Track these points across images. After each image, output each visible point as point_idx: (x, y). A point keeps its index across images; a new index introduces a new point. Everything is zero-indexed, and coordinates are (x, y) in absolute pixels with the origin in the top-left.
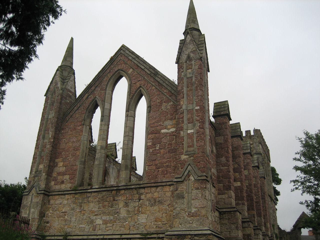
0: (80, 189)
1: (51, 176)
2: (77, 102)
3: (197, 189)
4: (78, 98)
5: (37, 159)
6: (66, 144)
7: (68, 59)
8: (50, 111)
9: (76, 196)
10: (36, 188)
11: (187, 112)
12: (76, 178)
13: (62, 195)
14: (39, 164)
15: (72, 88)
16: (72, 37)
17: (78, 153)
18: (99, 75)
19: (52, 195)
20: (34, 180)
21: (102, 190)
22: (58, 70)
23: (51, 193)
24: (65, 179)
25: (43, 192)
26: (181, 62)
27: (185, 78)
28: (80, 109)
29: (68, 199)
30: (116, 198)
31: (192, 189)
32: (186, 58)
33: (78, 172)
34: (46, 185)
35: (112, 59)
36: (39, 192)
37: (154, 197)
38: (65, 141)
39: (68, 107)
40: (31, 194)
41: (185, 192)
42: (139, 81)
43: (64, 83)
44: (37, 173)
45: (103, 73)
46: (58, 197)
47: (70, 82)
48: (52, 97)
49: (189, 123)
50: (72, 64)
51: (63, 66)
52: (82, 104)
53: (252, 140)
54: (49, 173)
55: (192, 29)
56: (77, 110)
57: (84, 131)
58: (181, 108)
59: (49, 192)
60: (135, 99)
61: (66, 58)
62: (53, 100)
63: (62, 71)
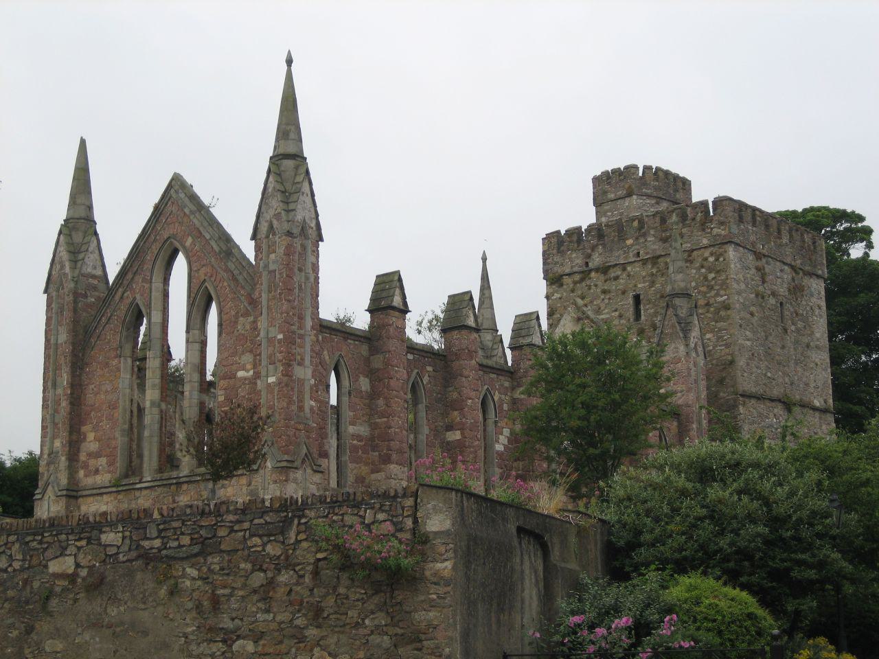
0: (124, 483)
1: (77, 461)
2: (105, 306)
3: (275, 482)
4: (113, 284)
5: (48, 430)
6: (96, 395)
7: (79, 201)
8: (59, 328)
9: (120, 497)
10: (53, 487)
11: (268, 342)
12: (117, 462)
13: (98, 494)
14: (54, 438)
15: (95, 268)
16: (82, 138)
17: (116, 415)
18: (139, 246)
19: (82, 496)
20: (48, 471)
21: (156, 483)
22: (60, 233)
23: (80, 493)
24: (101, 465)
25: (64, 493)
26: (258, 237)
27: (265, 274)
28: (111, 321)
29: (108, 503)
30: (176, 498)
31: (269, 483)
32: (266, 229)
33: (119, 451)
34: (68, 479)
35: (157, 208)
36: (59, 493)
37: (228, 495)
38: (93, 389)
39: (93, 313)
40: (46, 497)
41: (260, 488)
42: (204, 265)
43: (76, 262)
44: (52, 456)
45: (145, 242)
46: (92, 499)
47: (90, 255)
48: (58, 296)
49: (270, 364)
50: (90, 208)
51: (71, 221)
52: (114, 311)
53: (708, 233)
54: (73, 457)
55: (281, 157)
56: (107, 323)
57: (122, 370)
58: (259, 334)
59: (77, 491)
60: (198, 305)
61: (75, 198)
62: (62, 301)
63: (70, 232)
